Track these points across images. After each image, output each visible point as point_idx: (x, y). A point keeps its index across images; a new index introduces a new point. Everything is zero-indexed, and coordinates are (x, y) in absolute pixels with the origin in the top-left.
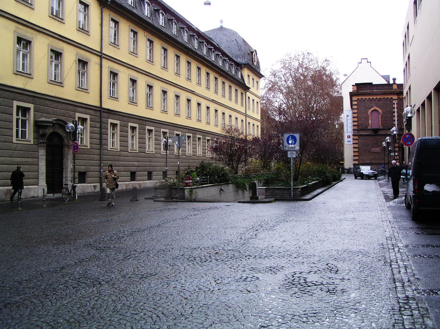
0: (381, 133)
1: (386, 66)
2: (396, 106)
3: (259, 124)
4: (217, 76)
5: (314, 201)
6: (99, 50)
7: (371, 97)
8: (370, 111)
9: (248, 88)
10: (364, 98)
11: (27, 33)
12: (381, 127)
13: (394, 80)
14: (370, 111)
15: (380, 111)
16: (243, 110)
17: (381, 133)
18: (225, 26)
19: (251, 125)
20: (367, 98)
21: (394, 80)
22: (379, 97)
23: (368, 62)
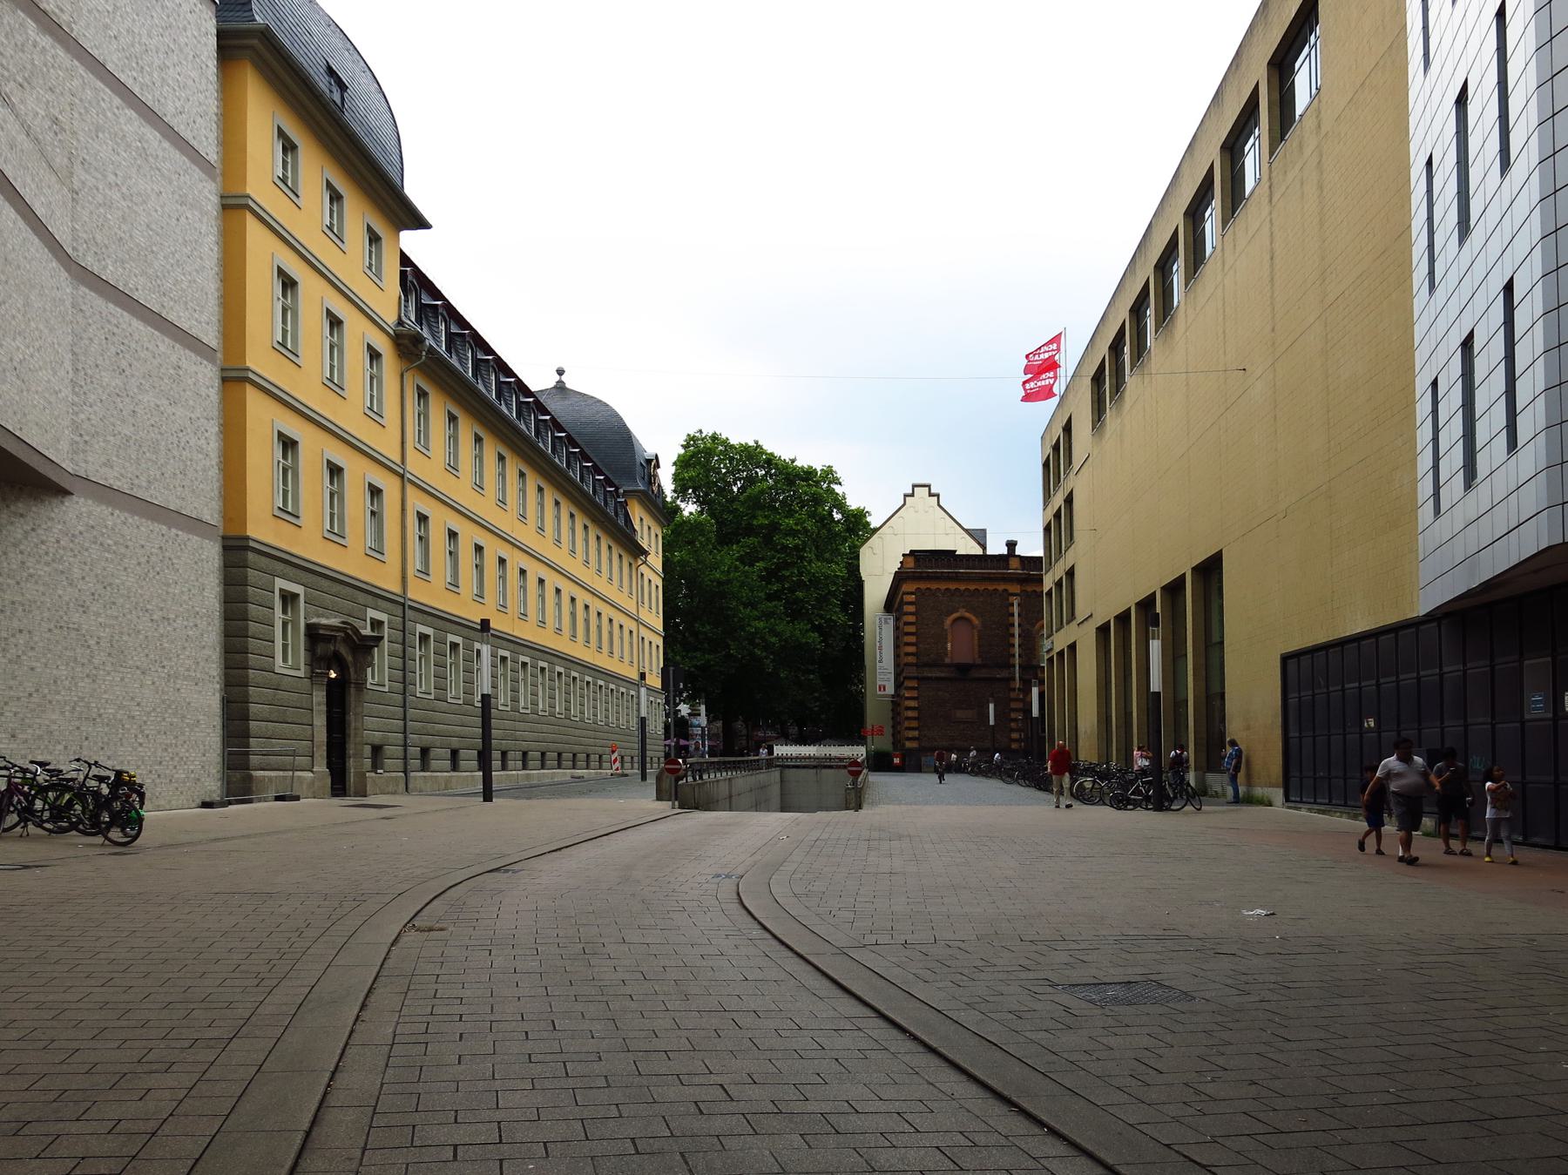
0: (975, 674)
1: (1005, 515)
2: (1016, 610)
3: (660, 642)
4: (589, 524)
5: (184, 364)
6: (396, 589)
7: (952, 586)
8: (948, 621)
9: (646, 553)
10: (934, 586)
11: (296, 269)
12: (979, 661)
13: (1011, 545)
14: (948, 621)
15: (976, 621)
16: (631, 606)
17: (975, 674)
18: (571, 382)
19: (616, 626)
20: (943, 586)
21: (1011, 545)
22: (972, 587)
23: (931, 495)
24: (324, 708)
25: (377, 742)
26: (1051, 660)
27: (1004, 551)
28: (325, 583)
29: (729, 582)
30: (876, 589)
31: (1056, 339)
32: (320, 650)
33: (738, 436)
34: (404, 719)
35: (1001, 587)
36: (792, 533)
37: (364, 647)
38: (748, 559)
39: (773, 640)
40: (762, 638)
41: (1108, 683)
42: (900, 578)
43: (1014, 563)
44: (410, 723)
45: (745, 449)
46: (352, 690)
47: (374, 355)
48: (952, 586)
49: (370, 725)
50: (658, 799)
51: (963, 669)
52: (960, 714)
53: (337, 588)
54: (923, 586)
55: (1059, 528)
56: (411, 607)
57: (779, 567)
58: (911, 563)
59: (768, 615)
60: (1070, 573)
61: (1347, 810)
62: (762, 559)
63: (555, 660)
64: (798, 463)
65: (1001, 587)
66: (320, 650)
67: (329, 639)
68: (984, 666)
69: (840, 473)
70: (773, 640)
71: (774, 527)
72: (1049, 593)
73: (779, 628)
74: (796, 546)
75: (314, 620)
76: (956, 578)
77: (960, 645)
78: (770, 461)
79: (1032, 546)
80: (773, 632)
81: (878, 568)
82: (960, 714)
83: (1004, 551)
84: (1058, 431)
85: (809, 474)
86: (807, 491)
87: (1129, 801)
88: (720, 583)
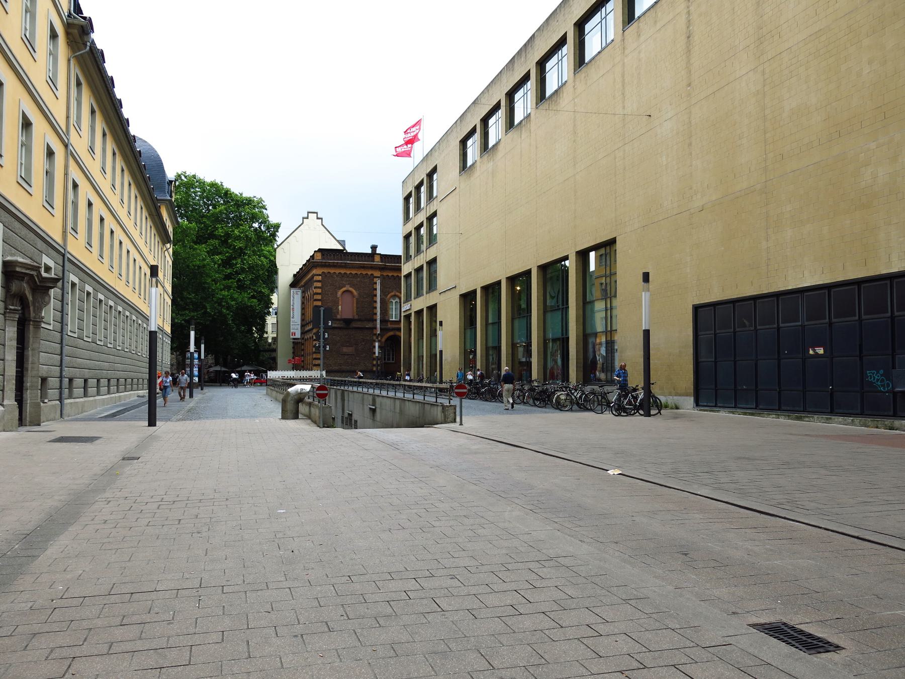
0: (354, 325)
1: (377, 231)
2: (378, 287)
7: (343, 271)
8: (340, 293)
10: (332, 271)
12: (356, 317)
13: (374, 248)
14: (340, 293)
15: (355, 293)
17: (354, 325)
20: (337, 271)
21: (374, 248)
22: (354, 272)
24: (15, 343)
25: (45, 375)
26: (408, 317)
27: (369, 251)
28: (17, 225)
29: (204, 266)
30: (285, 276)
31: (418, 123)
32: (14, 287)
33: (208, 177)
34: (61, 354)
35: (369, 273)
36: (238, 238)
37: (42, 287)
38: (212, 253)
39: (233, 303)
40: (227, 302)
41: (410, 330)
42: (310, 264)
43: (377, 258)
44: (65, 358)
45: (213, 185)
46: (31, 327)
47: (54, 36)
48: (343, 271)
49: (43, 361)
50: (284, 417)
51: (348, 322)
52: (345, 350)
53: (24, 232)
54: (326, 270)
55: (419, 236)
56: (69, 260)
57: (230, 259)
58: (319, 257)
59: (228, 288)
60: (433, 262)
61: (738, 410)
62: (220, 253)
63: (133, 311)
64: (244, 195)
65: (369, 273)
66: (14, 287)
67: (21, 277)
68: (359, 320)
69: (266, 203)
70: (233, 303)
71: (228, 235)
72: (408, 276)
73: (236, 296)
74: (240, 248)
75: (9, 258)
76: (345, 266)
77: (346, 308)
78: (227, 194)
79: (392, 246)
80: (233, 299)
81: (290, 259)
82: (345, 350)
83: (369, 251)
84: (422, 175)
85: (249, 201)
86: (244, 210)
87: (625, 410)
88: (199, 267)
